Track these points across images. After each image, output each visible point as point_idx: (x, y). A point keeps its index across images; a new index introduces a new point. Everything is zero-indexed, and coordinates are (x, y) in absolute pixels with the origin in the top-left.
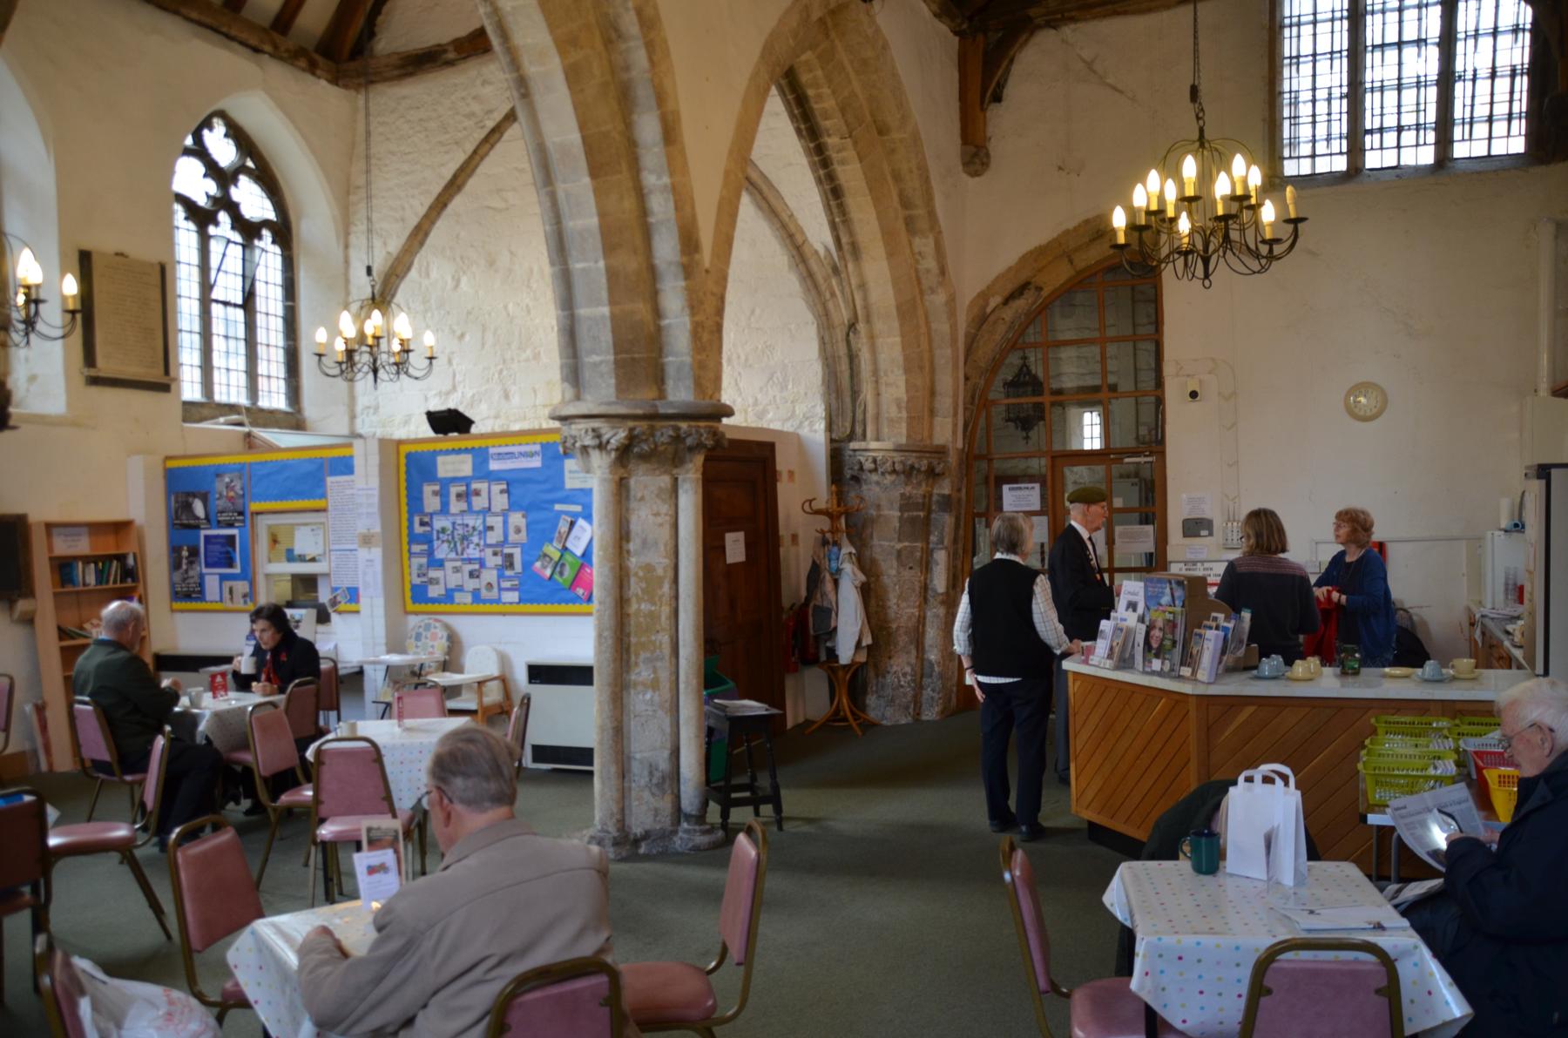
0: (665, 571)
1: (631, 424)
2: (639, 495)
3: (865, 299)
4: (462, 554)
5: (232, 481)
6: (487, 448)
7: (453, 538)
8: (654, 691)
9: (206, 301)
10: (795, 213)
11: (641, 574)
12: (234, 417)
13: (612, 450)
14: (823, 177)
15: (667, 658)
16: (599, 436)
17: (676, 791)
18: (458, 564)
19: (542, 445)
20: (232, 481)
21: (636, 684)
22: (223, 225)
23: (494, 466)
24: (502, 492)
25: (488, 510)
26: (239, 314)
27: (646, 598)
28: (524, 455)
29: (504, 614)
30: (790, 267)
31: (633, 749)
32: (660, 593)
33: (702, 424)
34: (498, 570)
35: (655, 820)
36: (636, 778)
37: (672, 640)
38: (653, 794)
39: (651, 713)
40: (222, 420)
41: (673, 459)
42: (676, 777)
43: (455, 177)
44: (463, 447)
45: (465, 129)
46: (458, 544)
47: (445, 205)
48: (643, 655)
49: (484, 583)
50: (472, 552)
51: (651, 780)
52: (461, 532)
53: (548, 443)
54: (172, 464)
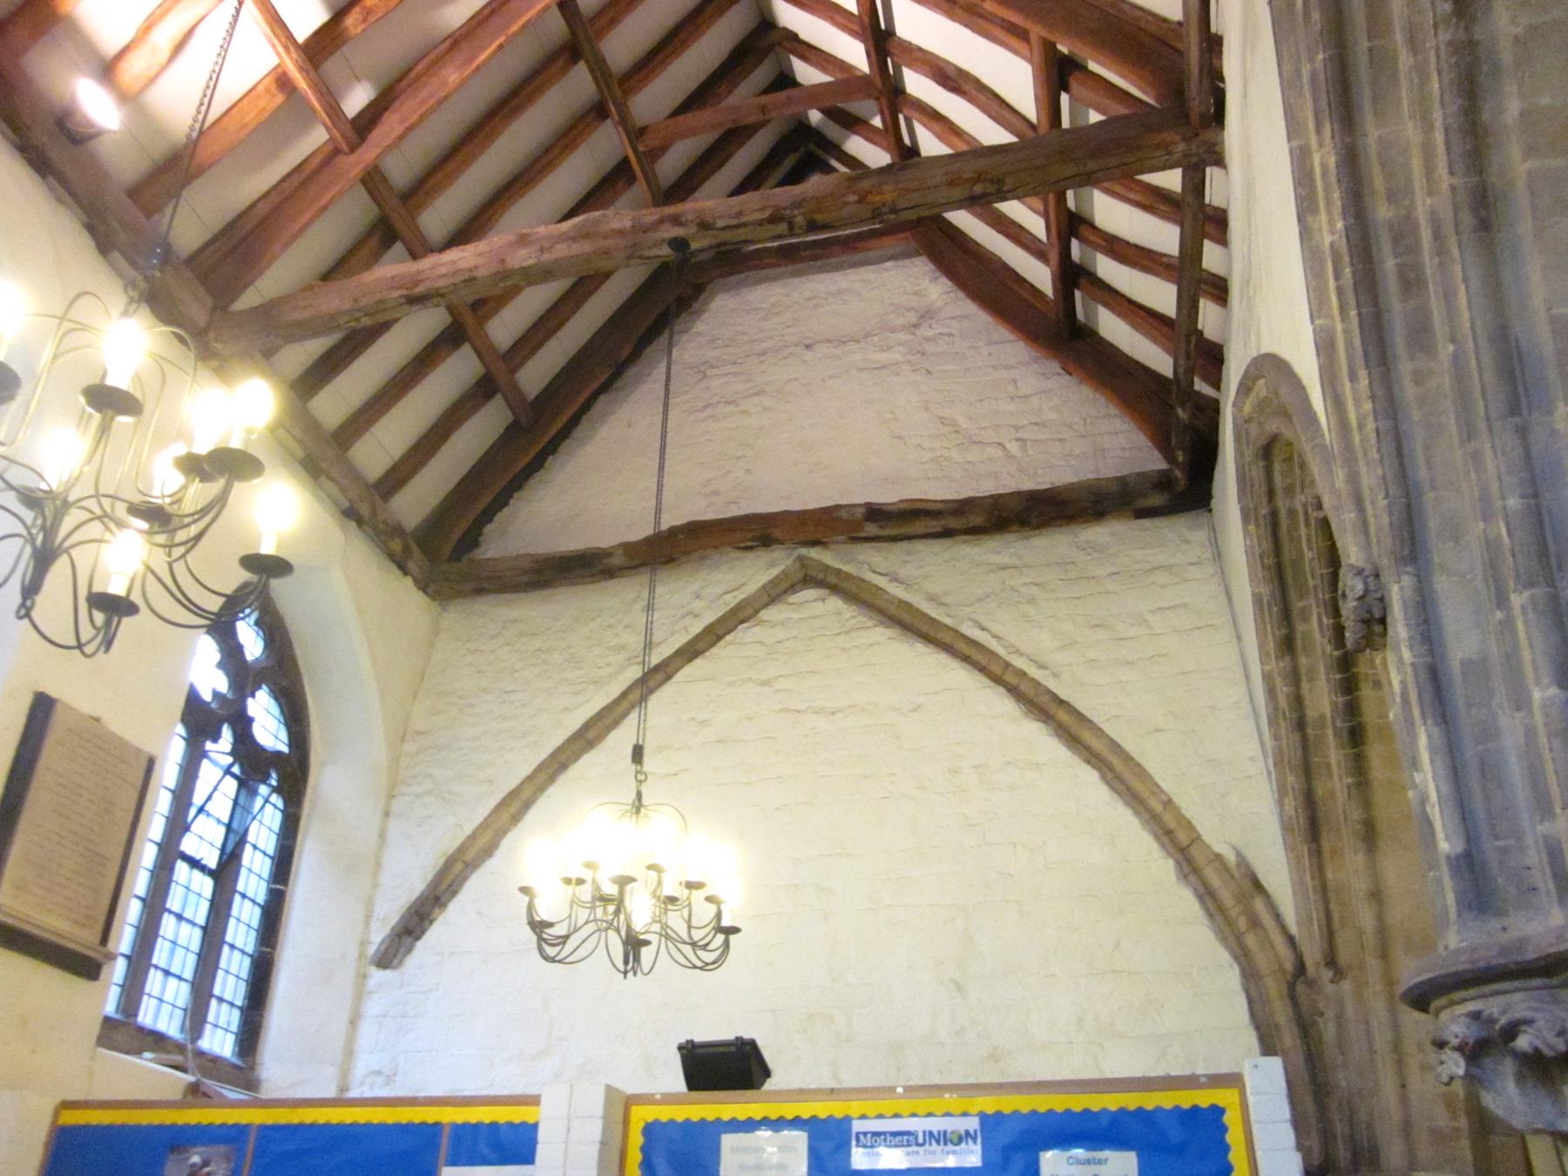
3: (1380, 917)
5: (206, 1163)
6: (847, 1120)
9: (170, 852)
10: (1175, 799)
12: (179, 1059)
14: (1340, 706)
19: (983, 1117)
20: (206, 1163)
22: (221, 748)
26: (206, 885)
28: (942, 1138)
30: (1178, 878)
40: (148, 1055)
43: (587, 726)
44: (790, 1116)
45: (609, 665)
47: (564, 767)
53: (999, 1114)
54: (71, 1118)
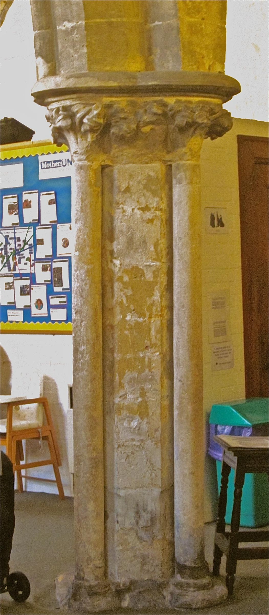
0: (155, 275)
1: (107, 100)
2: (124, 186)
4: (14, 270)
6: (37, 156)
7: (6, 253)
8: (142, 418)
11: (126, 279)
13: (86, 132)
15: (158, 377)
16: (72, 116)
17: (168, 536)
18: (10, 280)
21: (120, 409)
23: (44, 175)
24: (50, 202)
25: (36, 223)
27: (132, 307)
29: (54, 333)
31: (116, 485)
32: (149, 301)
33: (195, 99)
34: (47, 285)
35: (142, 568)
36: (120, 519)
37: (163, 358)
38: (140, 539)
39: (138, 444)
41: (165, 141)
42: (169, 521)
46: (11, 258)
48: (128, 375)
49: (34, 300)
50: (24, 268)
51: (137, 522)
52: (13, 246)
